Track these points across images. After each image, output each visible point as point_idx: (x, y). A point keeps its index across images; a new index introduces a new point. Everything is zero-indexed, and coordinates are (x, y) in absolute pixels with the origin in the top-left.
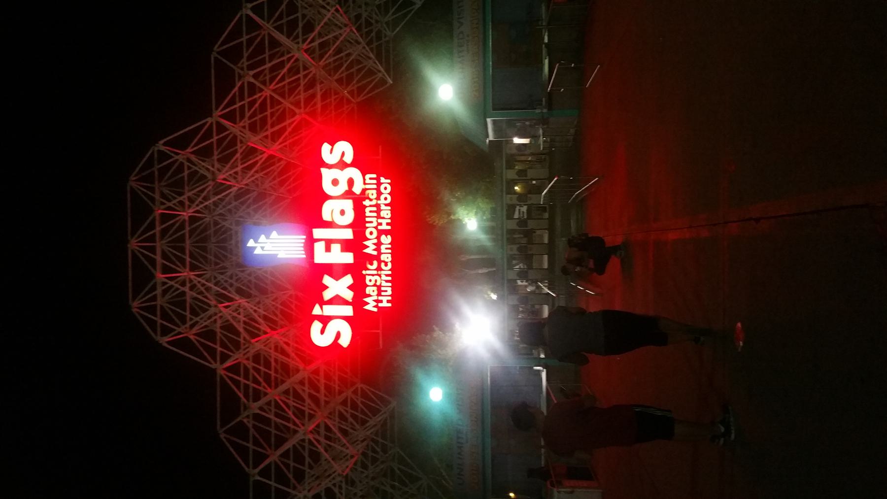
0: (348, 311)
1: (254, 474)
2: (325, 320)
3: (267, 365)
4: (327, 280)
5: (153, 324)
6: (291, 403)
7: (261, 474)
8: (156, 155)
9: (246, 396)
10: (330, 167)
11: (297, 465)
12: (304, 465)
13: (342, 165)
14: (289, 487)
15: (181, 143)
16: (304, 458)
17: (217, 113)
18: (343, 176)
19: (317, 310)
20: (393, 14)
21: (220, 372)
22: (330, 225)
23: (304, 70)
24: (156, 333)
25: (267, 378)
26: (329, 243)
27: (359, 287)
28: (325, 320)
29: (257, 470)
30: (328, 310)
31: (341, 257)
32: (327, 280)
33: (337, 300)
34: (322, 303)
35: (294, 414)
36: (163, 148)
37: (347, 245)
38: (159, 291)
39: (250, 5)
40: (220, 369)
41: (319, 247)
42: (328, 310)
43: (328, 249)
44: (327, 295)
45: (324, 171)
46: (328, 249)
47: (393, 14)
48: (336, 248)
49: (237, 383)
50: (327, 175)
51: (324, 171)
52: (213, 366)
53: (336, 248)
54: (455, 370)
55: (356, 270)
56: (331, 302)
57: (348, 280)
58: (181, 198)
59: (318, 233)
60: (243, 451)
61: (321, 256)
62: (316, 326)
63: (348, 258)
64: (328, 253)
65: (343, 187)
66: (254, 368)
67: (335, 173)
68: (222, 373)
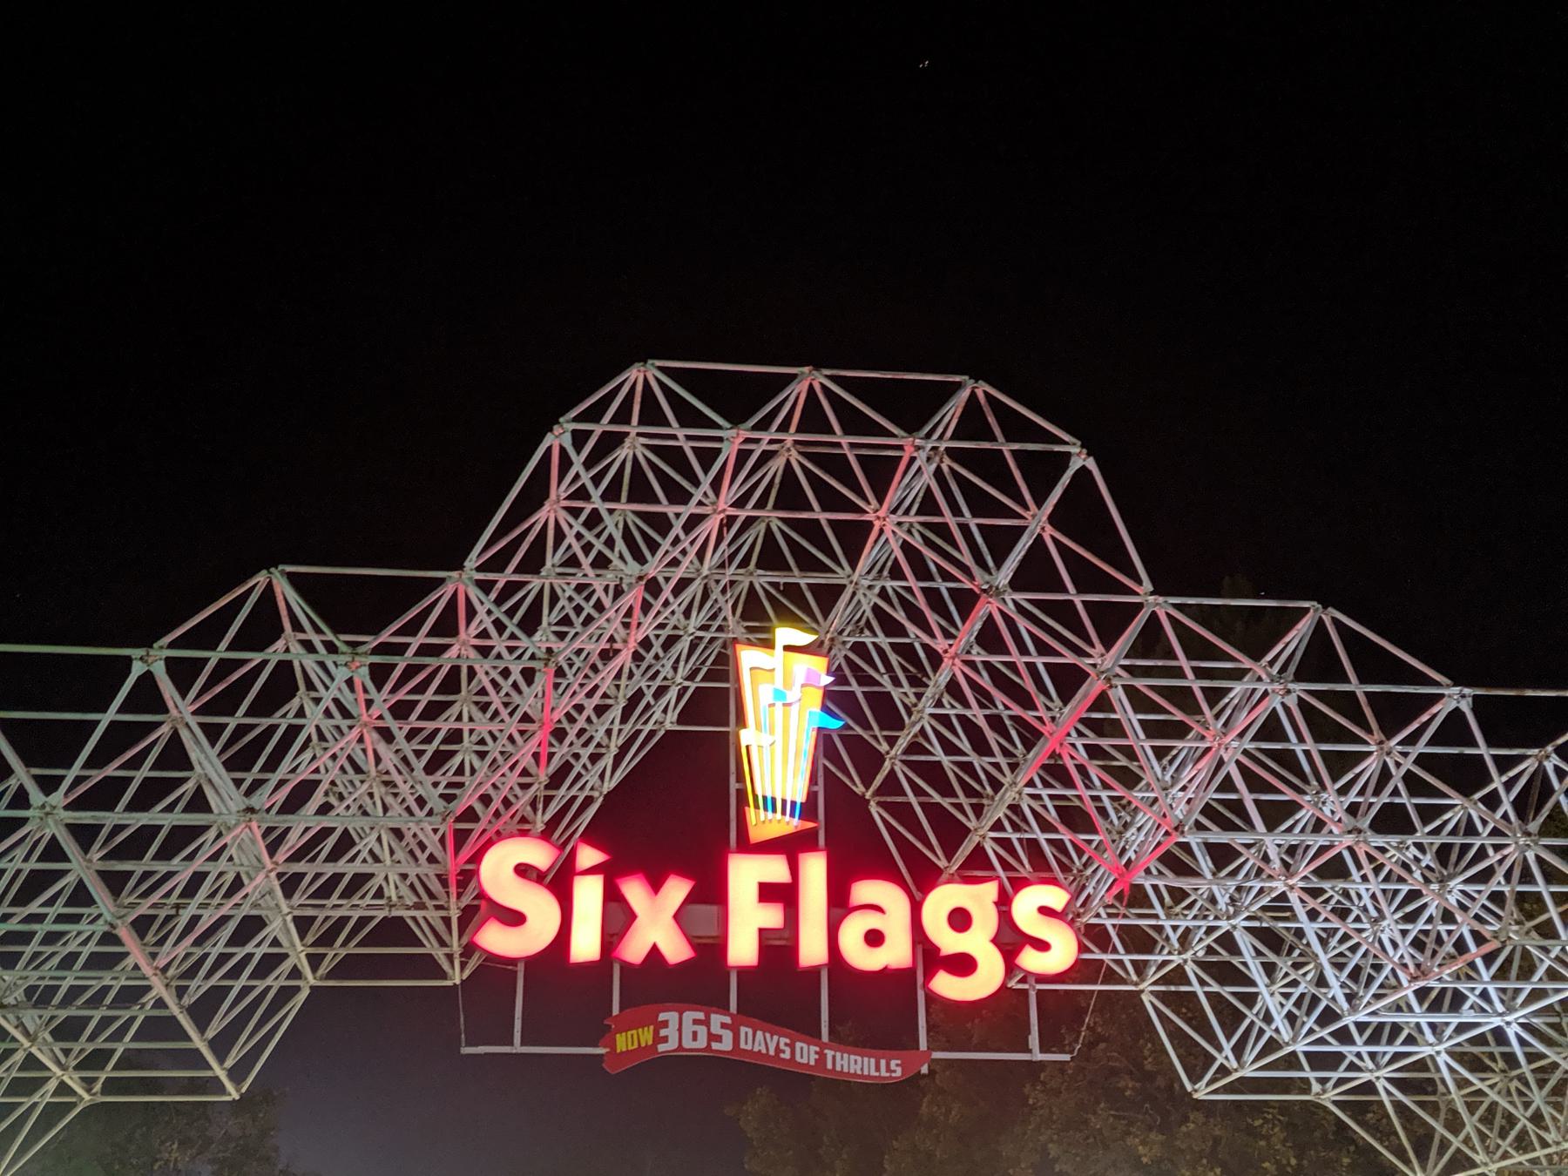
0: (586, 945)
1: (150, 661)
2: (560, 884)
4: (677, 890)
5: (594, 414)
7: (148, 678)
8: (1057, 448)
9: (382, 649)
10: (1004, 903)
13: (1011, 941)
14: (86, 766)
15: (1077, 513)
17: (1162, 606)
18: (978, 942)
19: (588, 856)
20: (1398, 1105)
21: (1144, 592)
22: (839, 904)
23: (1003, 829)
25: (225, 703)
26: (782, 895)
27: (655, 983)
28: (560, 884)
29: (159, 670)
30: (588, 893)
31: (746, 928)
32: (677, 890)
33: (618, 918)
34: (611, 875)
36: (1075, 465)
37: (778, 948)
38: (681, 436)
39: (1465, 706)
40: (461, 582)
41: (774, 869)
42: (588, 893)
43: (768, 893)
44: (634, 892)
46: (768, 893)
47: (1398, 1105)
48: (772, 916)
49: (411, 629)
52: (472, 561)
53: (772, 916)
57: (676, 950)
58: (671, 510)
59: (815, 869)
60: (207, 636)
61: (747, 875)
62: (539, 855)
63: (743, 949)
64: (753, 892)
65: (949, 942)
67: (985, 921)
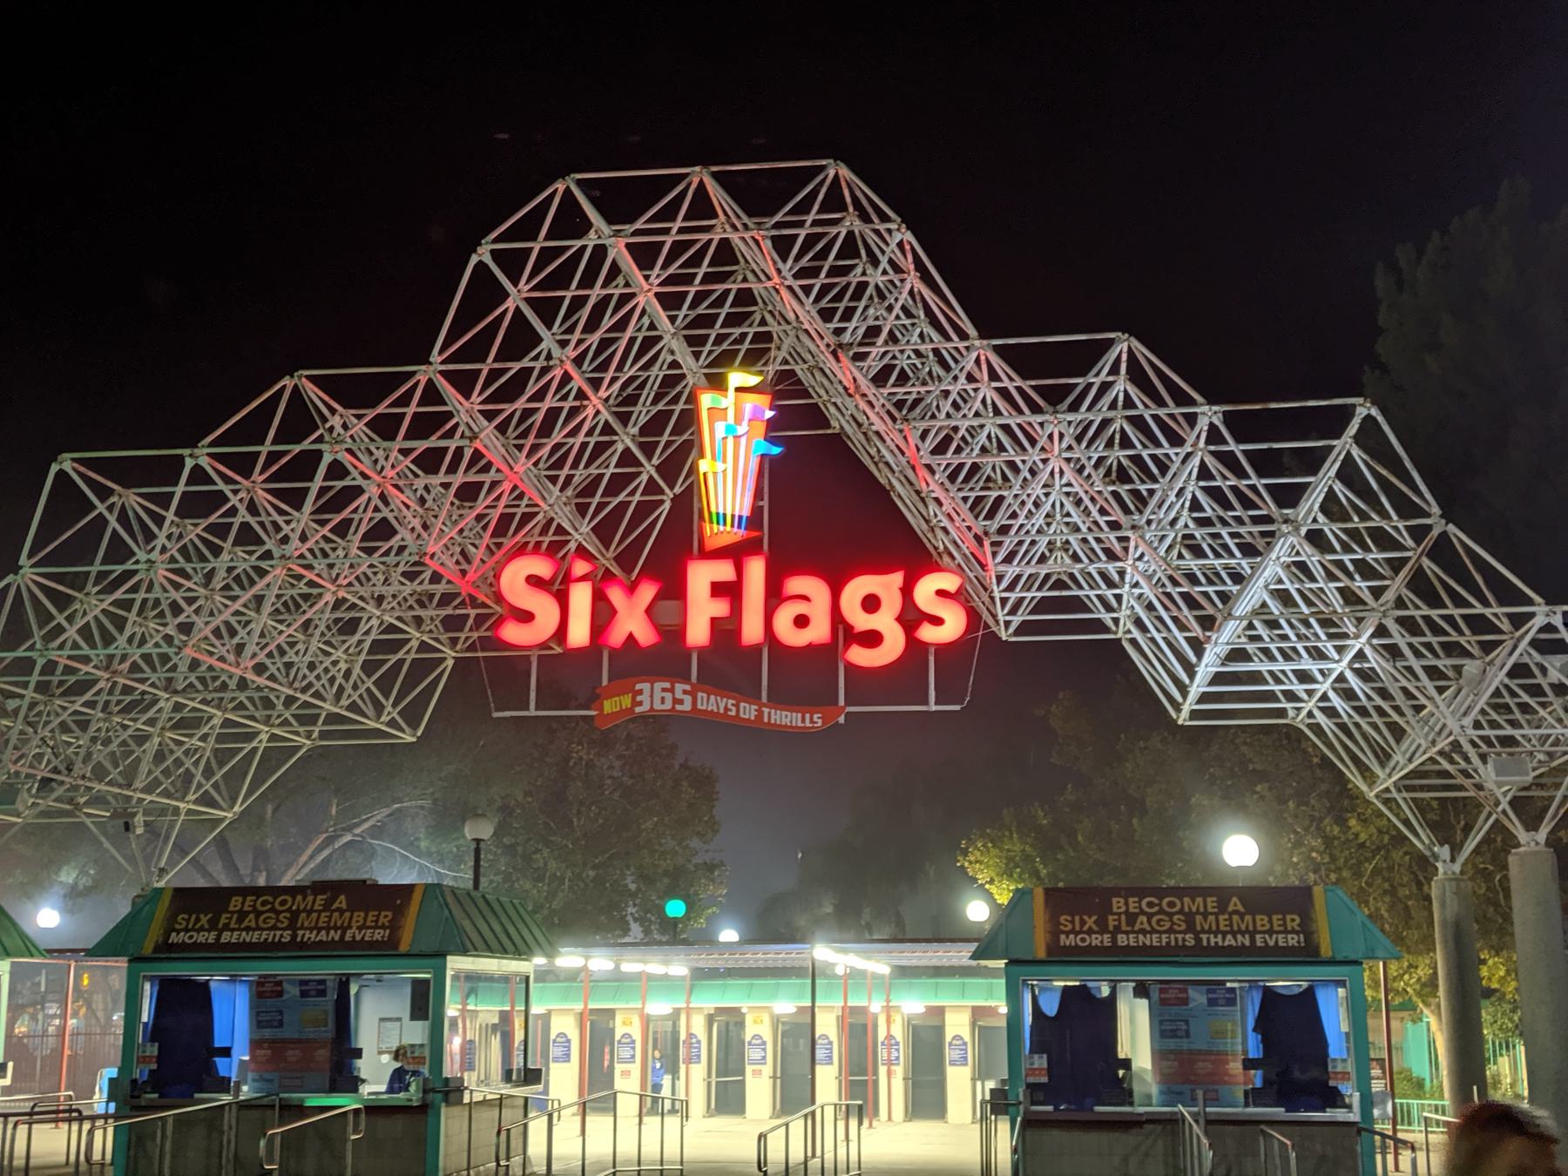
3: (733, 320)
5: (527, 229)
6: (654, 371)
10: (907, 591)
11: (567, 302)
12: (406, 438)
13: (911, 618)
16: (426, 437)
18: (885, 621)
22: (775, 595)
24: (495, 241)
26: (728, 591)
30: (581, 597)
33: (603, 615)
35: (632, 379)
37: (725, 631)
40: (432, 370)
41: (724, 571)
42: (581, 597)
45: (897, 579)
48: (721, 608)
50: (887, 586)
51: (897, 579)
52: (435, 357)
53: (721, 608)
54: (1482, 949)
55: (667, 654)
56: (599, 597)
57: (645, 635)
59: (756, 570)
61: (702, 576)
65: (861, 621)
66: (693, 306)
67: (892, 604)
68: (422, 379)
